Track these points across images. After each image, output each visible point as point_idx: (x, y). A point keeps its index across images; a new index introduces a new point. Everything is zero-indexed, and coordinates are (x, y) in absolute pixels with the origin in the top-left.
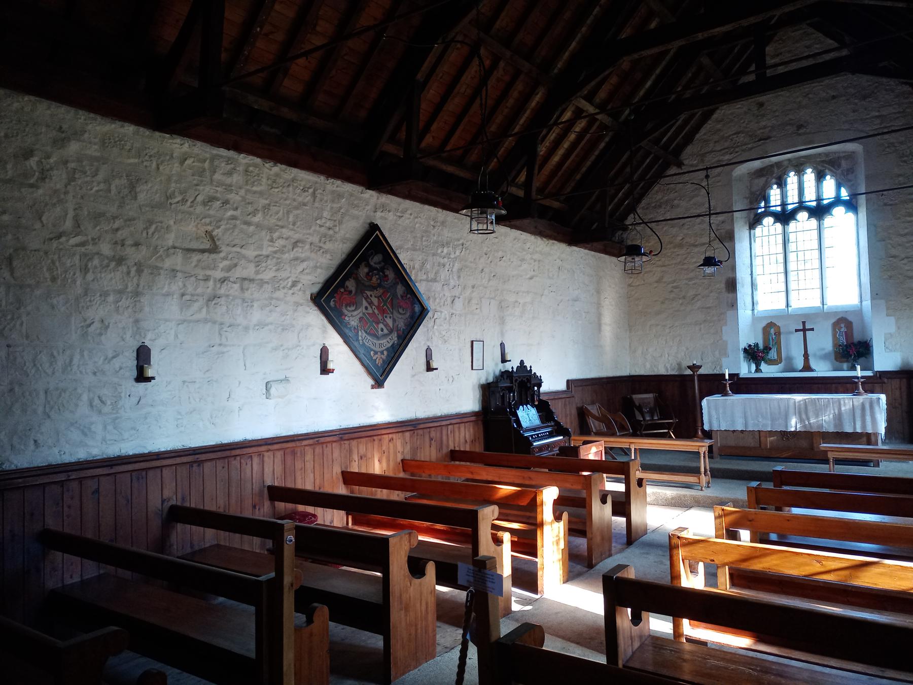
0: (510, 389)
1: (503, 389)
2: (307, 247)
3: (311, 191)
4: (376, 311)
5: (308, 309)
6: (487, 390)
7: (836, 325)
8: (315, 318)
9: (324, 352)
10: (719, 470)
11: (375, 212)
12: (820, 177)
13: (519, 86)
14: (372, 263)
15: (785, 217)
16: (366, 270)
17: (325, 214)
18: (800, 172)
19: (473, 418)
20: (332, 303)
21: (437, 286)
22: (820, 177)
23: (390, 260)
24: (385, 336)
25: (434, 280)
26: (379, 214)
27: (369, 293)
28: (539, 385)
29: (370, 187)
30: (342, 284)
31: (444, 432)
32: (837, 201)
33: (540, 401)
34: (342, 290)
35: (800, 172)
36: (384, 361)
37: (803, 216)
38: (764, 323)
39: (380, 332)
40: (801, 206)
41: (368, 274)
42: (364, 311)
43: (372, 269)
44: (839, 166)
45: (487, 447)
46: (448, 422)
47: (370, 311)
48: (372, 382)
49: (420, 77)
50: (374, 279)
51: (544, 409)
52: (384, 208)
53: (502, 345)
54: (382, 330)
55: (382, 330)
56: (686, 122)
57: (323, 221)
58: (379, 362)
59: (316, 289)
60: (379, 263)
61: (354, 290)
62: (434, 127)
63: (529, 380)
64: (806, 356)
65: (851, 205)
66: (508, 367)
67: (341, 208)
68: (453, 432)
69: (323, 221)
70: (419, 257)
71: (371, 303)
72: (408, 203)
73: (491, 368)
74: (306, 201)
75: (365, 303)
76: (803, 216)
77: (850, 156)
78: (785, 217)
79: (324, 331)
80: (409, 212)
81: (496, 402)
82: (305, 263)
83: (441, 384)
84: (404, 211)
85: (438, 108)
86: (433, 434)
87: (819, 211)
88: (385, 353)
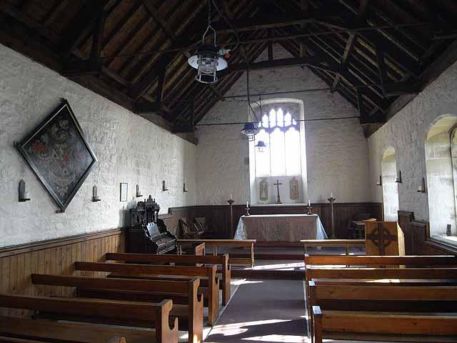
0: (143, 213)
1: (139, 212)
2: (13, 106)
3: (20, 67)
4: (62, 159)
5: (11, 152)
6: (129, 214)
7: (291, 182)
8: (13, 158)
9: (21, 186)
10: (258, 255)
11: (65, 91)
12: (285, 114)
13: (158, 36)
14: (61, 125)
15: (269, 130)
16: (56, 129)
17: (29, 85)
18: (276, 110)
19: (120, 232)
20: (30, 150)
21: (102, 147)
22: (285, 114)
23: (73, 124)
24: (67, 176)
25: (101, 142)
26: (67, 93)
27: (58, 146)
28: (158, 211)
29: (62, 74)
30: (38, 137)
31: (103, 242)
32: (292, 125)
33: (158, 220)
34: (39, 141)
35: (276, 110)
36: (65, 194)
37: (277, 130)
38: (260, 180)
39: (64, 174)
40: (277, 126)
41: (58, 132)
42: (53, 157)
43: (61, 129)
44: (292, 109)
45: (128, 249)
46: (105, 235)
47: (58, 158)
48: (56, 208)
49: (106, 7)
50: (62, 137)
51: (160, 223)
52: (71, 90)
53: (164, 182)
54: (65, 172)
55: (65, 172)
56: (228, 79)
57: (27, 90)
58: (62, 195)
59: (18, 138)
60: (66, 126)
61: (47, 142)
62: (138, 34)
63: (153, 208)
64: (279, 197)
65: (298, 128)
66: (141, 199)
67: (41, 83)
68: (108, 241)
69: (27, 90)
70: (91, 126)
71: (58, 153)
72: (87, 91)
73: (129, 199)
74: (15, 73)
75: (54, 152)
76: (277, 130)
77: (298, 105)
78: (269, 130)
79: (23, 171)
80: (87, 96)
81: (134, 222)
82: (10, 118)
83: (99, 213)
84: (84, 95)
85: (111, 35)
86: (96, 243)
87: (284, 129)
88: (67, 188)
